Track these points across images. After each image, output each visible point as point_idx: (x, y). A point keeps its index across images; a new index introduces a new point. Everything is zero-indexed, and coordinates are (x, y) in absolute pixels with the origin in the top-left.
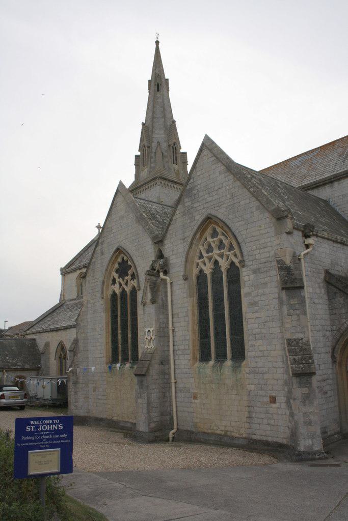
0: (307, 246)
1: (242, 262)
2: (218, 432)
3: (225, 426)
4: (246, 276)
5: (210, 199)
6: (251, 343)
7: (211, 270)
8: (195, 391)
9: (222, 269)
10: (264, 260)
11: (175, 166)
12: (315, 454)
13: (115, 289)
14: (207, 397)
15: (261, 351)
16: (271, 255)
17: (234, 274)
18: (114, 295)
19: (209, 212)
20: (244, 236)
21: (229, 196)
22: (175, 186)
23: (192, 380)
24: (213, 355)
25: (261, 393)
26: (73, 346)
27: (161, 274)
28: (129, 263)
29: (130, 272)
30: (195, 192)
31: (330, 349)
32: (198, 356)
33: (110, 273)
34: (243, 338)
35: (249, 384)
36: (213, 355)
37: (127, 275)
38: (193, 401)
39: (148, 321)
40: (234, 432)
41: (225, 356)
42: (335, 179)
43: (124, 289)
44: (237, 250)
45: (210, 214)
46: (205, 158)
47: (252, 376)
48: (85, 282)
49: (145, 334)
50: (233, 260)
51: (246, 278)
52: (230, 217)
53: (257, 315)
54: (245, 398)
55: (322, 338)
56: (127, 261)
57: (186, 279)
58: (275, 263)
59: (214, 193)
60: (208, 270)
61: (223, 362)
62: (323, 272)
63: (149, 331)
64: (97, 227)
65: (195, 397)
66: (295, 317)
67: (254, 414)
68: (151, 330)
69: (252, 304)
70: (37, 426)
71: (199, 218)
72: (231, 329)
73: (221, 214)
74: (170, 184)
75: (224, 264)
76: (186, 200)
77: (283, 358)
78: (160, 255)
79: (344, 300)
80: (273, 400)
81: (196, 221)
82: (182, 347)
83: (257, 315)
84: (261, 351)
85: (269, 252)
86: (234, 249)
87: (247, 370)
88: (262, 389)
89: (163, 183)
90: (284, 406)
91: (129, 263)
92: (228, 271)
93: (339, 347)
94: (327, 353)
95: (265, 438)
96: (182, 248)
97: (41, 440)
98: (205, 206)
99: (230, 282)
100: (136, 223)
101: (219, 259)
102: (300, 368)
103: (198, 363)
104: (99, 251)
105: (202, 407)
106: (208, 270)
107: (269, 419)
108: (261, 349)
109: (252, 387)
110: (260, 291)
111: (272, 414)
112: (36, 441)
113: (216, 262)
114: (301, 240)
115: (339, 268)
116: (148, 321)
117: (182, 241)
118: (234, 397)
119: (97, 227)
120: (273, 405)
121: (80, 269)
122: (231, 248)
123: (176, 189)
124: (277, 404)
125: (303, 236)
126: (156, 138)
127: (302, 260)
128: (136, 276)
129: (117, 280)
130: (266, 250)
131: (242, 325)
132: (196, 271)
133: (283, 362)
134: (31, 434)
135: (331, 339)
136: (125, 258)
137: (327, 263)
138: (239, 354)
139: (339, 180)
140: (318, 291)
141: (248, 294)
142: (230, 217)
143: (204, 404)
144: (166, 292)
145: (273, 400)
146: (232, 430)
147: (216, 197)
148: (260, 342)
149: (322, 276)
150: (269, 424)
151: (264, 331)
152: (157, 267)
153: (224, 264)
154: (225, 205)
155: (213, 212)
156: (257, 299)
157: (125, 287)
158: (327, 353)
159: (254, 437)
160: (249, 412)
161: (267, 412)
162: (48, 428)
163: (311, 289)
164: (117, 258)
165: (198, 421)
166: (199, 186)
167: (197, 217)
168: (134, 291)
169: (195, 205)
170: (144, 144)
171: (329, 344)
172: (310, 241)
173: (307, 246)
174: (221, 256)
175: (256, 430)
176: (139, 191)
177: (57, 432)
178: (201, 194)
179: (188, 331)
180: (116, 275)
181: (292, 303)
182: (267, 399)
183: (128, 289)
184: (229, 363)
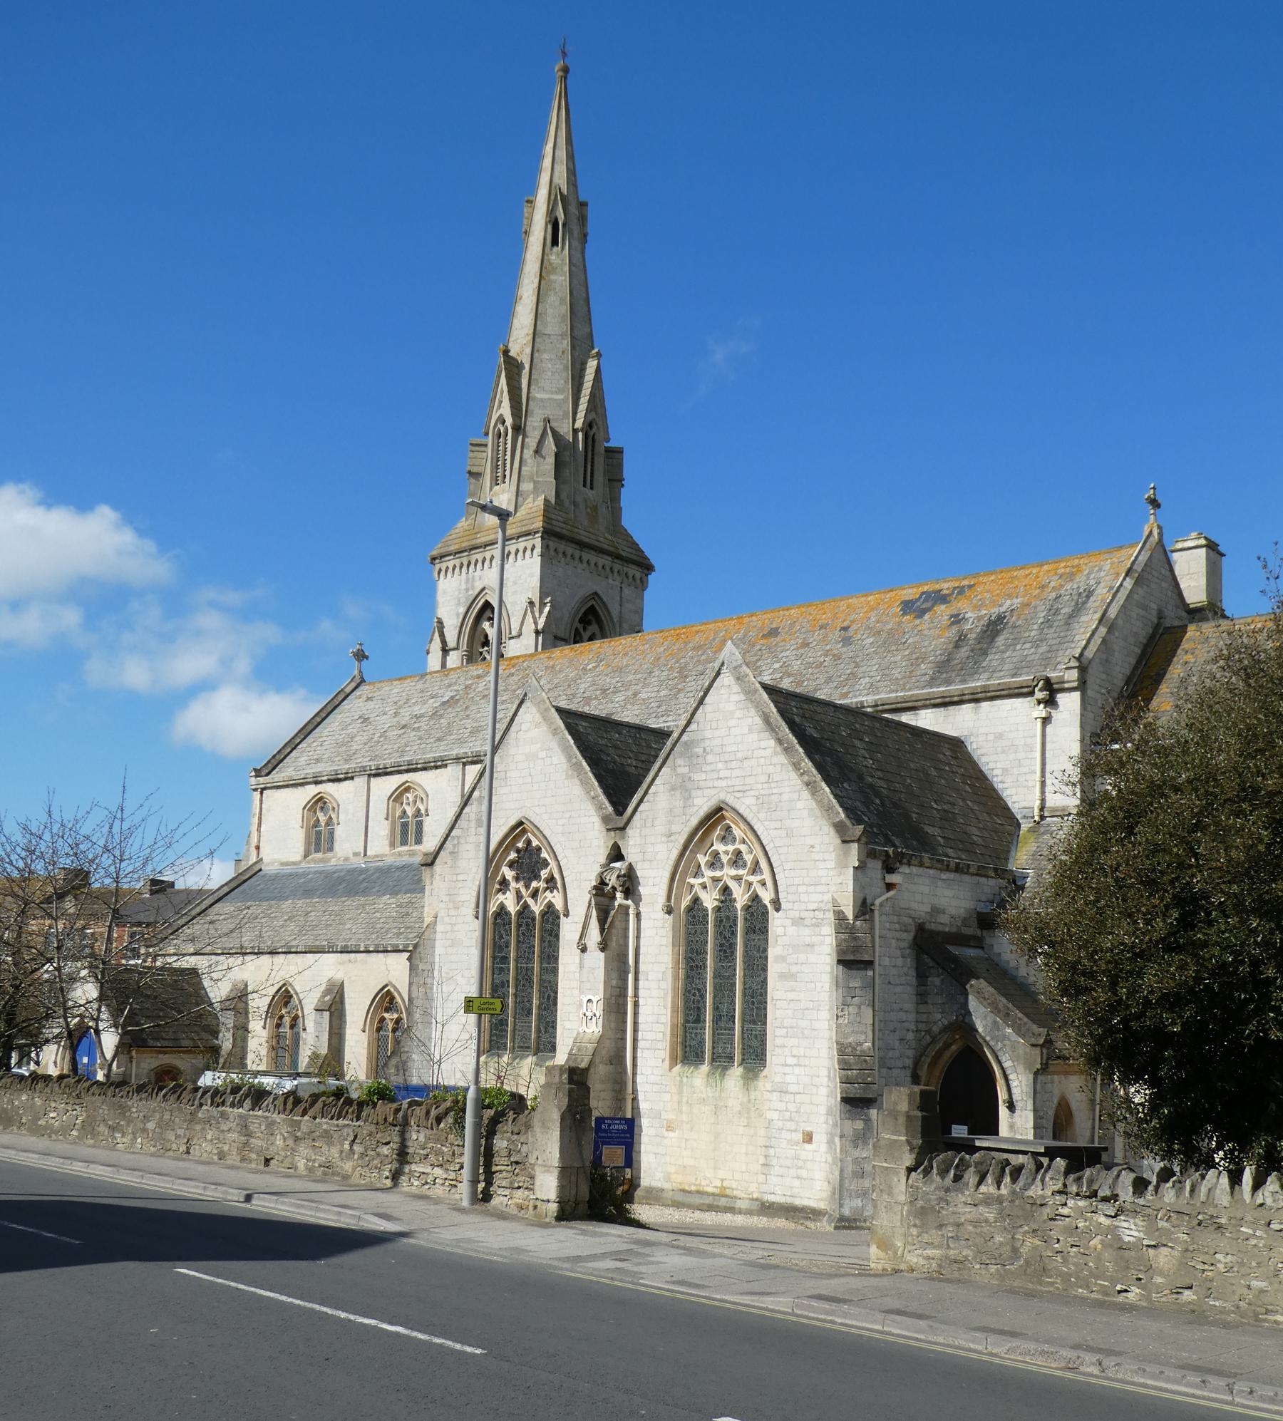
0: (890, 887)
1: (777, 905)
2: (710, 1190)
3: (722, 1180)
4: (777, 923)
5: (727, 773)
6: (779, 1041)
7: (716, 903)
8: (671, 1116)
9: (739, 905)
10: (815, 906)
11: (587, 490)
12: (865, 1221)
13: (506, 903)
14: (691, 1129)
15: (794, 1056)
16: (825, 901)
17: (758, 917)
18: (502, 911)
19: (722, 796)
20: (783, 857)
21: (763, 778)
22: (585, 556)
23: (667, 1097)
24: (707, 1056)
25: (789, 1125)
26: (328, 998)
27: (619, 895)
28: (544, 855)
29: (544, 874)
30: (699, 751)
31: (909, 1062)
32: (679, 1053)
33: (498, 868)
34: (765, 1030)
35: (770, 1110)
36: (707, 1056)
37: (537, 877)
38: (666, 1134)
39: (589, 981)
40: (737, 1189)
41: (730, 1058)
42: (983, 695)
43: (526, 906)
44: (767, 875)
45: (723, 802)
46: (723, 691)
47: (775, 1096)
48: (432, 876)
49: (581, 1006)
50: (759, 893)
51: (780, 931)
52: (762, 816)
53: (791, 995)
54: (762, 1132)
55: (897, 1043)
56: (539, 849)
57: (669, 911)
58: (831, 916)
59: (734, 765)
60: (710, 900)
61: (725, 1068)
62: (913, 928)
63: (589, 1001)
64: (367, 658)
65: (670, 1128)
66: (853, 1010)
67: (774, 1162)
68: (595, 1001)
69: (785, 977)
70: (609, 1125)
71: (702, 806)
72: (743, 1013)
73: (745, 805)
74: (570, 551)
75: (741, 898)
76: (680, 761)
77: (829, 1073)
78: (616, 854)
79: (942, 981)
80: (808, 1138)
81: (696, 808)
82: (650, 1036)
83: (791, 995)
84: (794, 1056)
85: (822, 893)
86: (761, 873)
87: (769, 1086)
88: (791, 1119)
89: (561, 551)
90: (824, 1148)
91: (544, 855)
92: (747, 908)
93: (927, 1060)
94: (905, 1068)
95: (789, 1200)
96: (666, 853)
97: (611, 1137)
98: (717, 783)
99: (749, 930)
100: (567, 779)
101: (733, 885)
102: (855, 1090)
103: (679, 1066)
104: (473, 816)
105: (683, 1145)
106: (710, 900)
107: (800, 1168)
108: (795, 1052)
109: (775, 1115)
110: (802, 957)
111: (804, 1161)
112: (608, 1137)
113: (726, 890)
114: (879, 876)
115: (944, 919)
116: (589, 981)
117: (664, 839)
118: (741, 1130)
119: (367, 658)
120: (807, 1146)
121: (316, 783)
122: (756, 869)
123: (585, 565)
124: (814, 1144)
125: (883, 868)
126: (542, 400)
127: (877, 913)
128: (559, 885)
129: (513, 885)
130: (819, 888)
131: (765, 1009)
132: (686, 901)
133: (829, 1077)
134: (605, 1131)
135: (913, 1044)
136: (535, 843)
137: (921, 908)
138: (755, 1055)
139: (992, 698)
140: (900, 962)
141: (782, 959)
142: (762, 816)
143: (686, 1140)
144: (627, 929)
145: (808, 1138)
146: (734, 1186)
147: (738, 772)
148: (794, 1042)
149: (909, 937)
150: (798, 1178)
151: (803, 1024)
152: (612, 880)
153: (741, 898)
154: (752, 793)
155: (731, 800)
156: (794, 969)
157: (530, 901)
158: (905, 1068)
159: (772, 1198)
160: (766, 1156)
161: (797, 1158)
162: (617, 1127)
163: (887, 959)
164: (516, 839)
165: (673, 1171)
166: (707, 743)
167: (698, 801)
168: (551, 916)
169: (697, 777)
170: (501, 415)
171: (910, 1053)
172: (893, 878)
173: (890, 887)
174: (738, 879)
175: (775, 1186)
176: (480, 557)
177: (623, 1131)
178: (710, 758)
179: (665, 1007)
180: (509, 874)
181: (851, 985)
182: (799, 1137)
183: (537, 908)
184: (736, 1071)
